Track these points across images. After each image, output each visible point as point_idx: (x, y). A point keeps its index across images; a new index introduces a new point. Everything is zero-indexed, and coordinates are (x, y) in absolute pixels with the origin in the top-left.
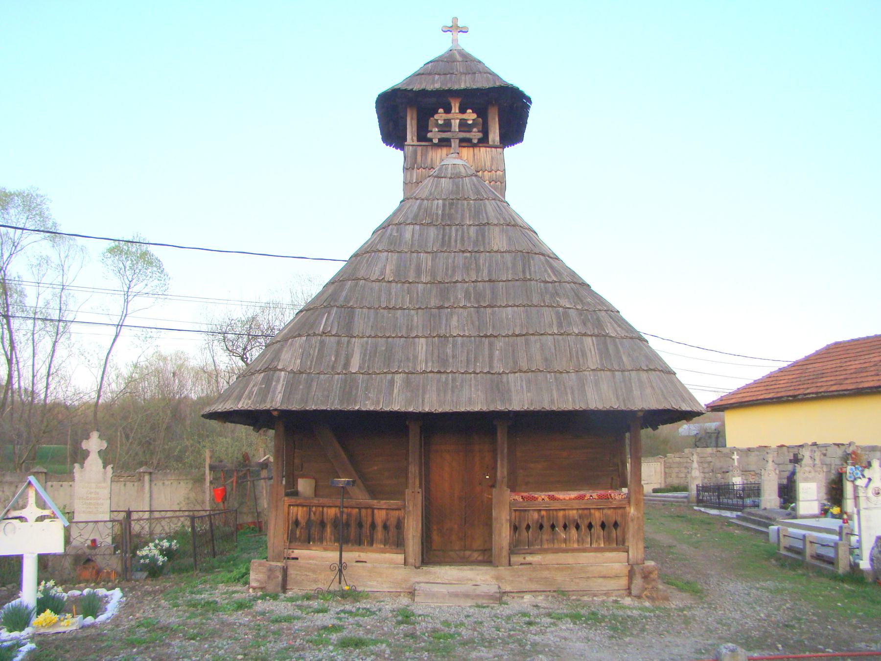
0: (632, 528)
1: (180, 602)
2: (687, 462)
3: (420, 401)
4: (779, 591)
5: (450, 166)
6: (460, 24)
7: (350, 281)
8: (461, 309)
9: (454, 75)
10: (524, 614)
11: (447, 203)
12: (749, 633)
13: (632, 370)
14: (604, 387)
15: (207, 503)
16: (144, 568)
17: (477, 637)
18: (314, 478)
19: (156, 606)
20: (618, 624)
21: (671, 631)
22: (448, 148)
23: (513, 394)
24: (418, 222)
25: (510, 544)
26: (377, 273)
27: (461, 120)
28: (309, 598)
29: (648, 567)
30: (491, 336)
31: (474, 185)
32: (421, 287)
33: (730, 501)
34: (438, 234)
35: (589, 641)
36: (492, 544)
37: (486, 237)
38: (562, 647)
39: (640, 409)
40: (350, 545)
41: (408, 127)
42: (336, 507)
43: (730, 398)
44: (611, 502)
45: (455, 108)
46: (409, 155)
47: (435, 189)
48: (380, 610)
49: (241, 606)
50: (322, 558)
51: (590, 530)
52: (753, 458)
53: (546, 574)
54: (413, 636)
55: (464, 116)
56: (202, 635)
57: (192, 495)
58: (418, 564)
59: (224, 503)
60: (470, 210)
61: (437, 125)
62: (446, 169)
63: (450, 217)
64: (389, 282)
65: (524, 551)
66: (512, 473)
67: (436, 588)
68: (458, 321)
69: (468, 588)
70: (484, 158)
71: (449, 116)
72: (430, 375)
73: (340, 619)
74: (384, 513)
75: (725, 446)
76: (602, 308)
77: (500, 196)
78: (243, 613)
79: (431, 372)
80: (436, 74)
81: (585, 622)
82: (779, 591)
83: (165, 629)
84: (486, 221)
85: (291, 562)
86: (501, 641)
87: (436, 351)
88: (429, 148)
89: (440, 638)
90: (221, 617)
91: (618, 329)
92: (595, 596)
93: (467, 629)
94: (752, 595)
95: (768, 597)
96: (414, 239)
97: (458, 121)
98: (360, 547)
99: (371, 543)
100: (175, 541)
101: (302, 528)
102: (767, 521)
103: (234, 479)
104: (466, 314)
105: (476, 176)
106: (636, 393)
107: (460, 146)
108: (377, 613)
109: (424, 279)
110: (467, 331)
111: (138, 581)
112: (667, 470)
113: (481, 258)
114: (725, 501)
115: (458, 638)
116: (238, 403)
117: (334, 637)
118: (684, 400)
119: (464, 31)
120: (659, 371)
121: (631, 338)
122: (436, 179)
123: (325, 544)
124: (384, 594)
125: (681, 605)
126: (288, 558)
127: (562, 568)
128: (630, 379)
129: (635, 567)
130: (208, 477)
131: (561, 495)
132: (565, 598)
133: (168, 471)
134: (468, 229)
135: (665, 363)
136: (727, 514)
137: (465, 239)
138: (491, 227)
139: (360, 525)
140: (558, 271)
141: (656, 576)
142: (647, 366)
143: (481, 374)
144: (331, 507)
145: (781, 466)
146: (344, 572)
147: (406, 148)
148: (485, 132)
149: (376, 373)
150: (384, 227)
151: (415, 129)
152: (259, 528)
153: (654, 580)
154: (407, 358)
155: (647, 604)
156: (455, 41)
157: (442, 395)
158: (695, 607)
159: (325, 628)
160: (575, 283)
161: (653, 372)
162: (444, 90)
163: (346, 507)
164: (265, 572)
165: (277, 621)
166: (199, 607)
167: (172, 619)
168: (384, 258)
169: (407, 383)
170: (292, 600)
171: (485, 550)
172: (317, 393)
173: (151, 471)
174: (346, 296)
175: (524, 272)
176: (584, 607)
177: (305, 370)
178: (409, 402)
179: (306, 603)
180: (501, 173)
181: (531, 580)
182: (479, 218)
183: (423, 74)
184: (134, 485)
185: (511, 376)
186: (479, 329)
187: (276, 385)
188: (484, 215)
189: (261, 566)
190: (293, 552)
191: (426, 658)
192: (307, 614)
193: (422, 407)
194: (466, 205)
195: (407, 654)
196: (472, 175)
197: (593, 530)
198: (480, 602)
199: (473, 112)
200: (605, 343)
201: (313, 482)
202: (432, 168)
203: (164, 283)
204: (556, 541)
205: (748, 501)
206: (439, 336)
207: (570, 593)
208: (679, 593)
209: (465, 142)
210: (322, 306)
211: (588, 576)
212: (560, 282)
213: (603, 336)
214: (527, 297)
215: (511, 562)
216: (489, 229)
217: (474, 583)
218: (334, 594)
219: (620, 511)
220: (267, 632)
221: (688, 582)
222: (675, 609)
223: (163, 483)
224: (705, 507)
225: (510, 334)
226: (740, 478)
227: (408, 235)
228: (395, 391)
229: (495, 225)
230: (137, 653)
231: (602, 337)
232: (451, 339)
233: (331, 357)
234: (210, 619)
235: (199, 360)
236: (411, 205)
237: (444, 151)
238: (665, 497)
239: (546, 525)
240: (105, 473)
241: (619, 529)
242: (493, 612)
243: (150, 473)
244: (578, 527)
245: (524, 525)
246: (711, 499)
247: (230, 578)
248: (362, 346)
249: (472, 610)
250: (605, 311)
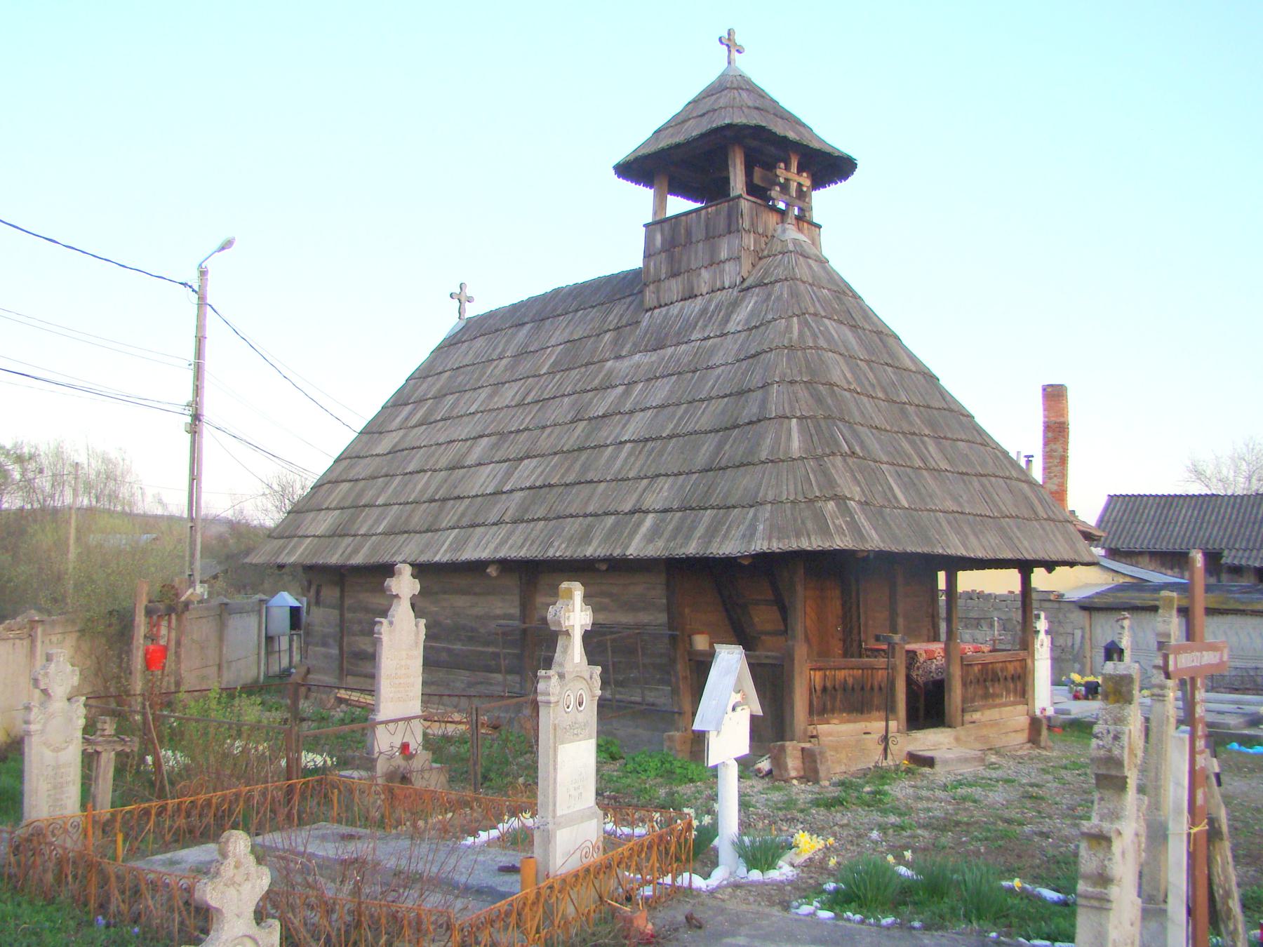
45: (794, 168)
97: (795, 184)
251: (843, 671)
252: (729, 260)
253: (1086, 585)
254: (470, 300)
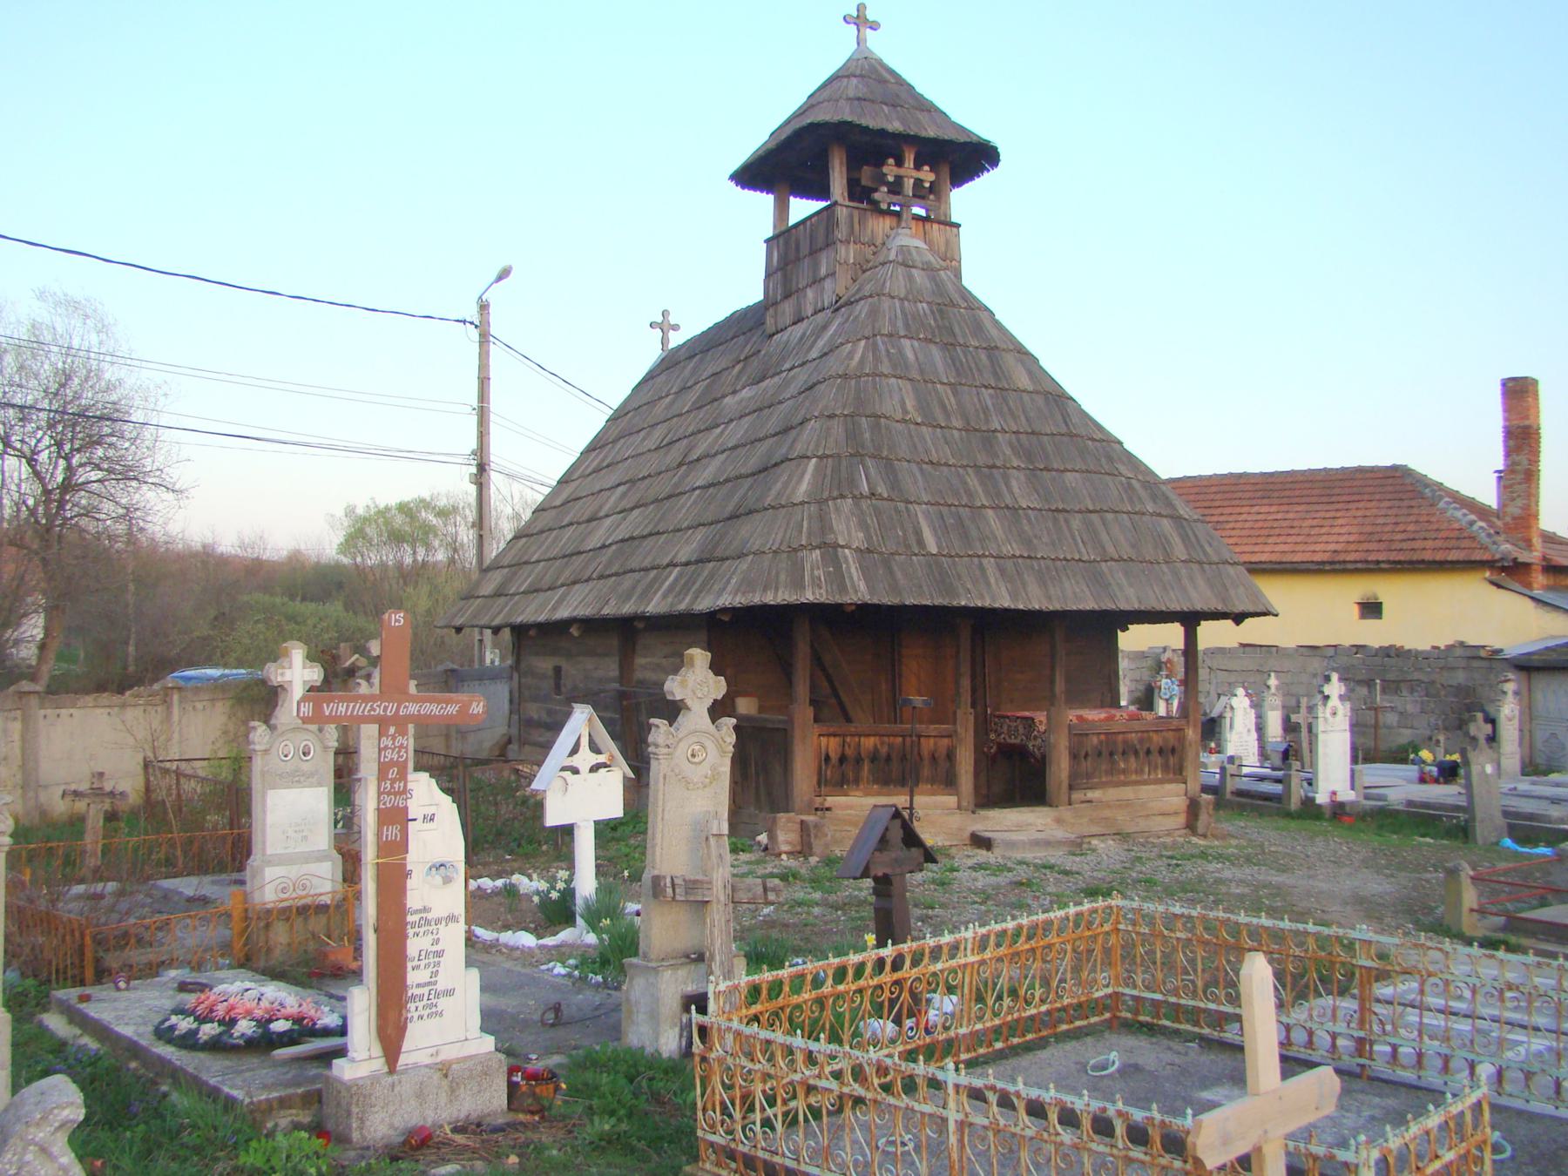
45: (909, 162)
53: (1107, 813)
58: (972, 807)
71: (902, 172)
97: (912, 181)
119: (874, 26)
144: (869, 735)
149: (958, 555)
181: (1092, 821)
223: (194, 707)
228: (992, 581)
245: (1083, 753)
251: (872, 739)
252: (827, 276)
253: (1553, 637)
254: (675, 328)
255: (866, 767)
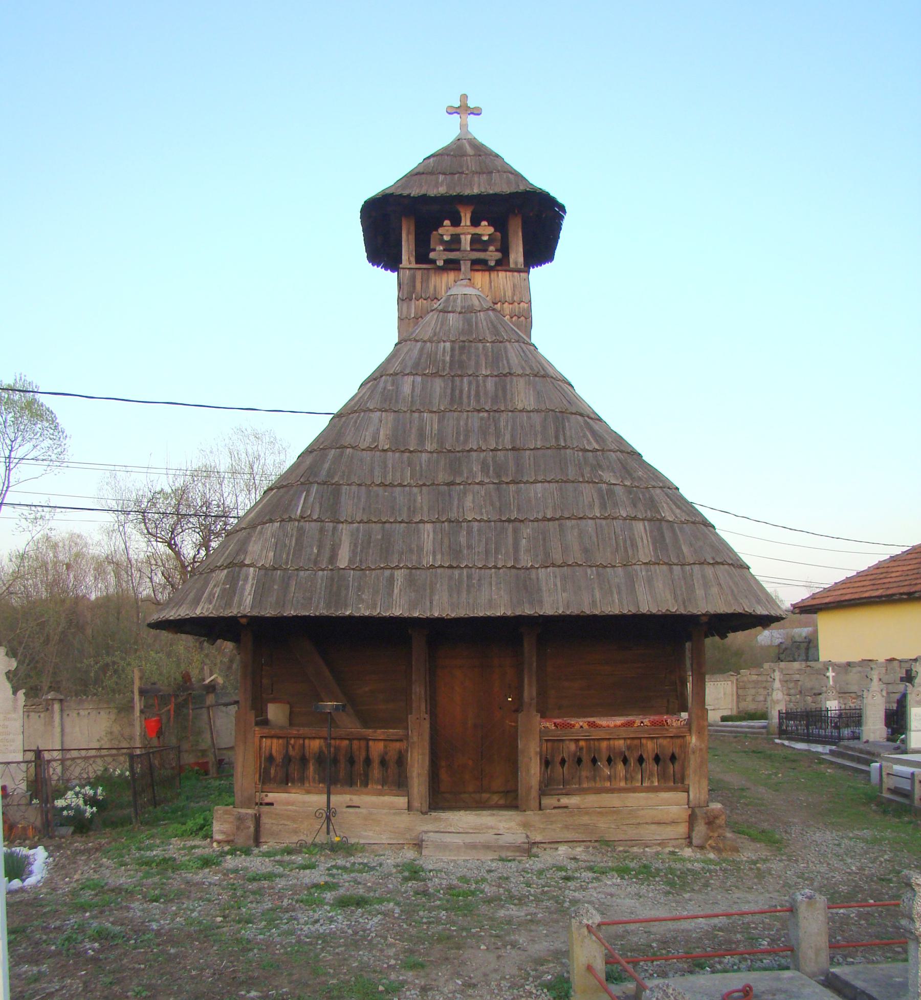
0: (693, 762)
1: (127, 859)
2: (767, 681)
3: (428, 603)
4: (875, 841)
5: (459, 297)
6: (471, 104)
7: (334, 450)
8: (476, 486)
9: (464, 176)
10: (560, 869)
11: (457, 347)
12: (836, 888)
13: (694, 564)
14: (659, 584)
15: (138, 738)
16: (68, 821)
17: (504, 894)
18: (288, 703)
19: (97, 866)
20: (676, 878)
21: (741, 887)
22: (456, 272)
23: (545, 595)
24: (420, 372)
25: (541, 782)
26: (369, 439)
27: (473, 235)
28: (290, 852)
29: (713, 810)
30: (516, 520)
31: (492, 322)
32: (424, 456)
33: (822, 732)
34: (445, 388)
35: (640, 897)
36: (517, 782)
37: (508, 391)
38: (609, 904)
39: (704, 612)
40: (339, 786)
41: (403, 243)
42: (320, 738)
43: (825, 595)
44: (667, 730)
45: (466, 220)
46: (406, 282)
47: (441, 328)
48: (381, 865)
49: (206, 862)
50: (304, 802)
51: (641, 765)
52: (853, 676)
53: (585, 819)
54: (425, 893)
55: (478, 230)
56: (166, 896)
57: (116, 729)
59: (159, 737)
60: (486, 356)
61: (442, 242)
62: (455, 301)
63: (462, 365)
64: (384, 451)
65: (559, 792)
66: (542, 693)
67: (448, 838)
68: (473, 502)
69: (488, 837)
70: (504, 286)
71: (457, 230)
72: (439, 571)
73: (333, 876)
74: (381, 745)
75: (818, 660)
76: (656, 485)
77: (525, 337)
78: (210, 871)
79: (441, 566)
80: (440, 173)
81: (636, 876)
82: (875, 841)
83: (118, 890)
84: (507, 370)
85: (265, 809)
86: (533, 898)
87: (446, 541)
88: (432, 273)
89: (458, 896)
90: (184, 876)
91: (678, 511)
92: (647, 847)
93: (490, 885)
94: (843, 846)
95: (862, 848)
96: (415, 394)
97: (469, 237)
98: (351, 789)
99: (365, 784)
100: (101, 788)
101: (277, 765)
102: (868, 757)
103: (172, 707)
104: (483, 493)
105: (494, 310)
106: (700, 592)
107: (472, 270)
108: (378, 868)
109: (428, 447)
110: (485, 515)
111: (63, 837)
112: (740, 692)
113: (501, 419)
114: (815, 731)
115: (481, 895)
116: (196, 608)
117: (329, 896)
118: (759, 601)
119: (477, 112)
120: (729, 564)
121: (693, 523)
122: (441, 313)
123: (308, 785)
124: (383, 846)
125: (754, 858)
126: (261, 804)
127: (605, 812)
128: (692, 575)
129: (697, 810)
130: (138, 705)
131: (603, 722)
132: (610, 849)
133: (85, 697)
134: (484, 382)
135: (735, 554)
136: (819, 748)
137: (481, 394)
138: (515, 378)
139: (351, 761)
140: (600, 437)
141: (723, 822)
142: (713, 559)
143: (504, 569)
144: (314, 738)
145: (890, 686)
146: (333, 820)
147: (401, 271)
148: (505, 250)
149: (370, 569)
150: (374, 379)
151: (412, 247)
152: (223, 767)
153: (720, 827)
154: (410, 550)
155: (712, 856)
156: (464, 126)
157: (455, 596)
158: (771, 859)
159: (316, 886)
160: (622, 452)
161: (721, 566)
162: (451, 196)
163: (334, 739)
164: (232, 822)
165: (254, 879)
166: (154, 865)
167: (123, 878)
168: (377, 421)
169: (411, 582)
170: (268, 854)
171: (508, 792)
172: (297, 595)
173: (62, 697)
174: (330, 469)
175: (557, 438)
176: (633, 859)
177: (281, 566)
178: (413, 605)
179: (287, 858)
180: (526, 306)
181: (567, 827)
182: (498, 367)
183: (423, 173)
184: (39, 716)
185: (542, 572)
186: (500, 511)
187: (244, 585)
188: (505, 362)
189: (226, 814)
190: (267, 796)
191: (444, 917)
192: (291, 870)
193: (431, 612)
194: (481, 348)
195: (421, 913)
196: (488, 309)
197: (644, 765)
198: (504, 854)
199: (489, 225)
200: (660, 530)
201: (288, 706)
202: (436, 298)
203: (59, 443)
204: (597, 778)
205: (846, 732)
206: (450, 521)
207: (616, 843)
208: (752, 844)
209: (479, 265)
210: (299, 483)
211: (638, 821)
212: (603, 450)
213: (658, 520)
214: (561, 469)
215: (542, 805)
216: (511, 382)
217: (496, 831)
218: (322, 847)
219: (678, 741)
220: (245, 892)
221: (763, 831)
222: (747, 862)
223: (79, 714)
224: (788, 739)
225: (540, 518)
226: (836, 702)
227: (406, 389)
228: (396, 591)
229: (519, 375)
230: (92, 917)
231: (657, 521)
232: (464, 525)
233: (313, 549)
234: (170, 878)
235: (106, 547)
236: (410, 350)
237: (452, 276)
238: (737, 727)
239: (586, 759)
240: (15, 700)
241: (677, 765)
242: (521, 867)
243: (61, 701)
244: (625, 761)
245: (558, 759)
246: (797, 730)
247: (185, 831)
248: (352, 535)
249: (494, 865)
250: (661, 487)
255: (311, 768)
